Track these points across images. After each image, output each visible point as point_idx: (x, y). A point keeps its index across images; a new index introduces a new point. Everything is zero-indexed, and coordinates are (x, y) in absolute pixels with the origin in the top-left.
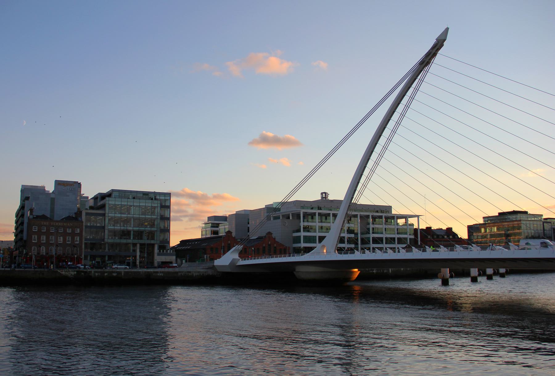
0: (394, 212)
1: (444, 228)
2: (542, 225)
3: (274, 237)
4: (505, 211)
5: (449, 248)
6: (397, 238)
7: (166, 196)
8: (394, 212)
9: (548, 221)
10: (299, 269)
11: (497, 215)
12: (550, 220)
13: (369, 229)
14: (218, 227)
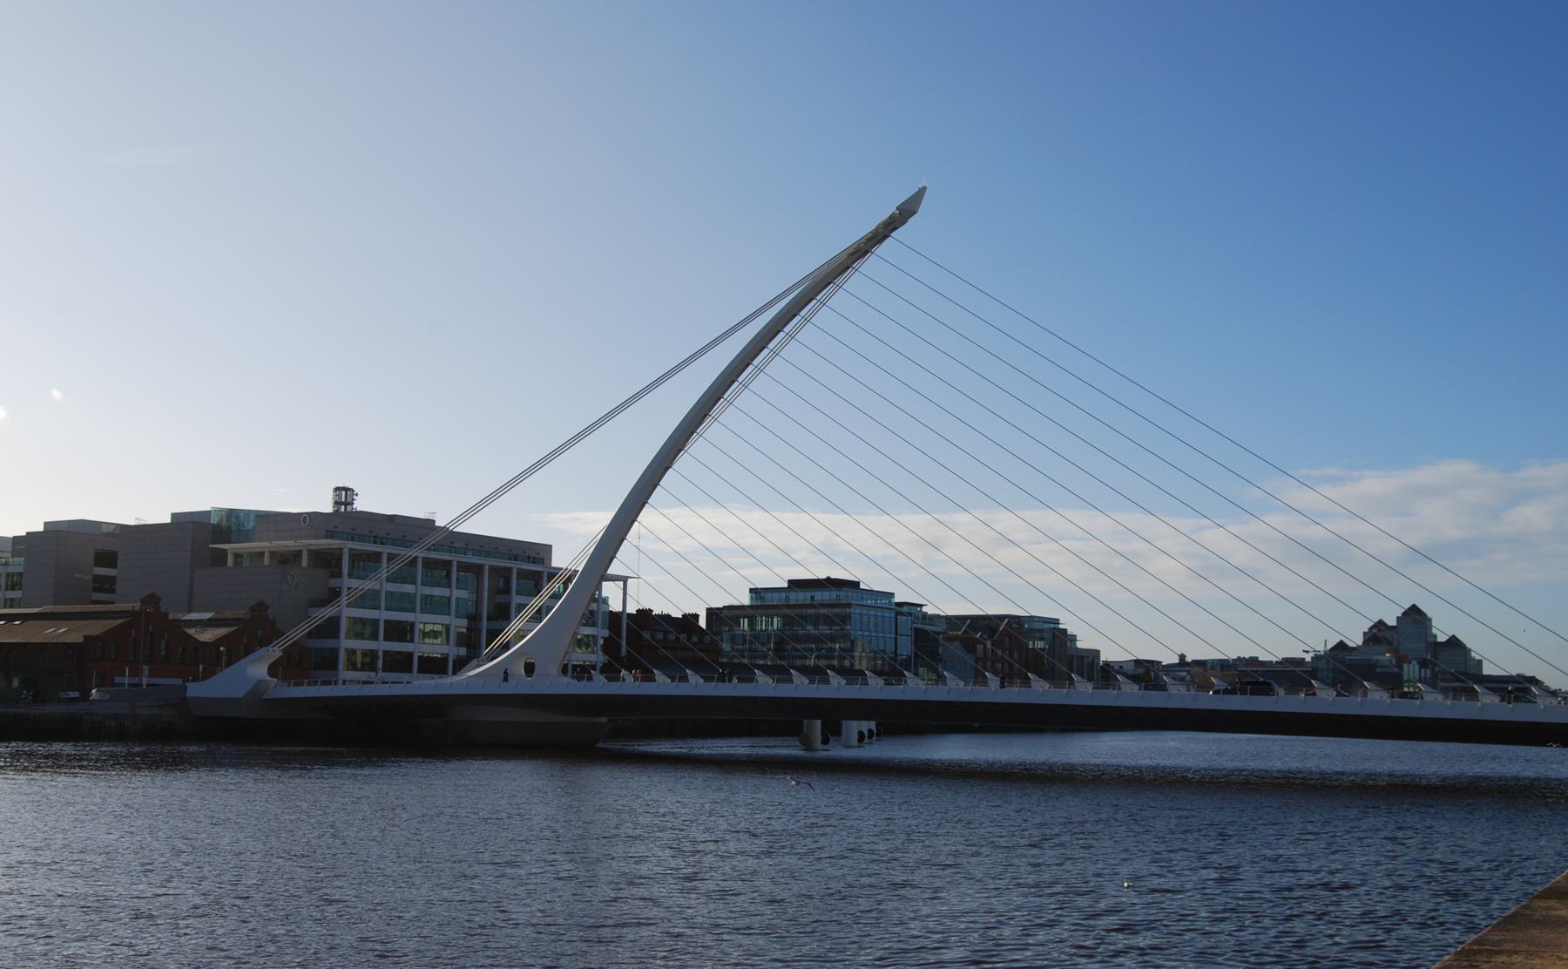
2: (893, 620)
3: (271, 618)
5: (776, 677)
9: (905, 609)
11: (786, 585)
12: (908, 607)
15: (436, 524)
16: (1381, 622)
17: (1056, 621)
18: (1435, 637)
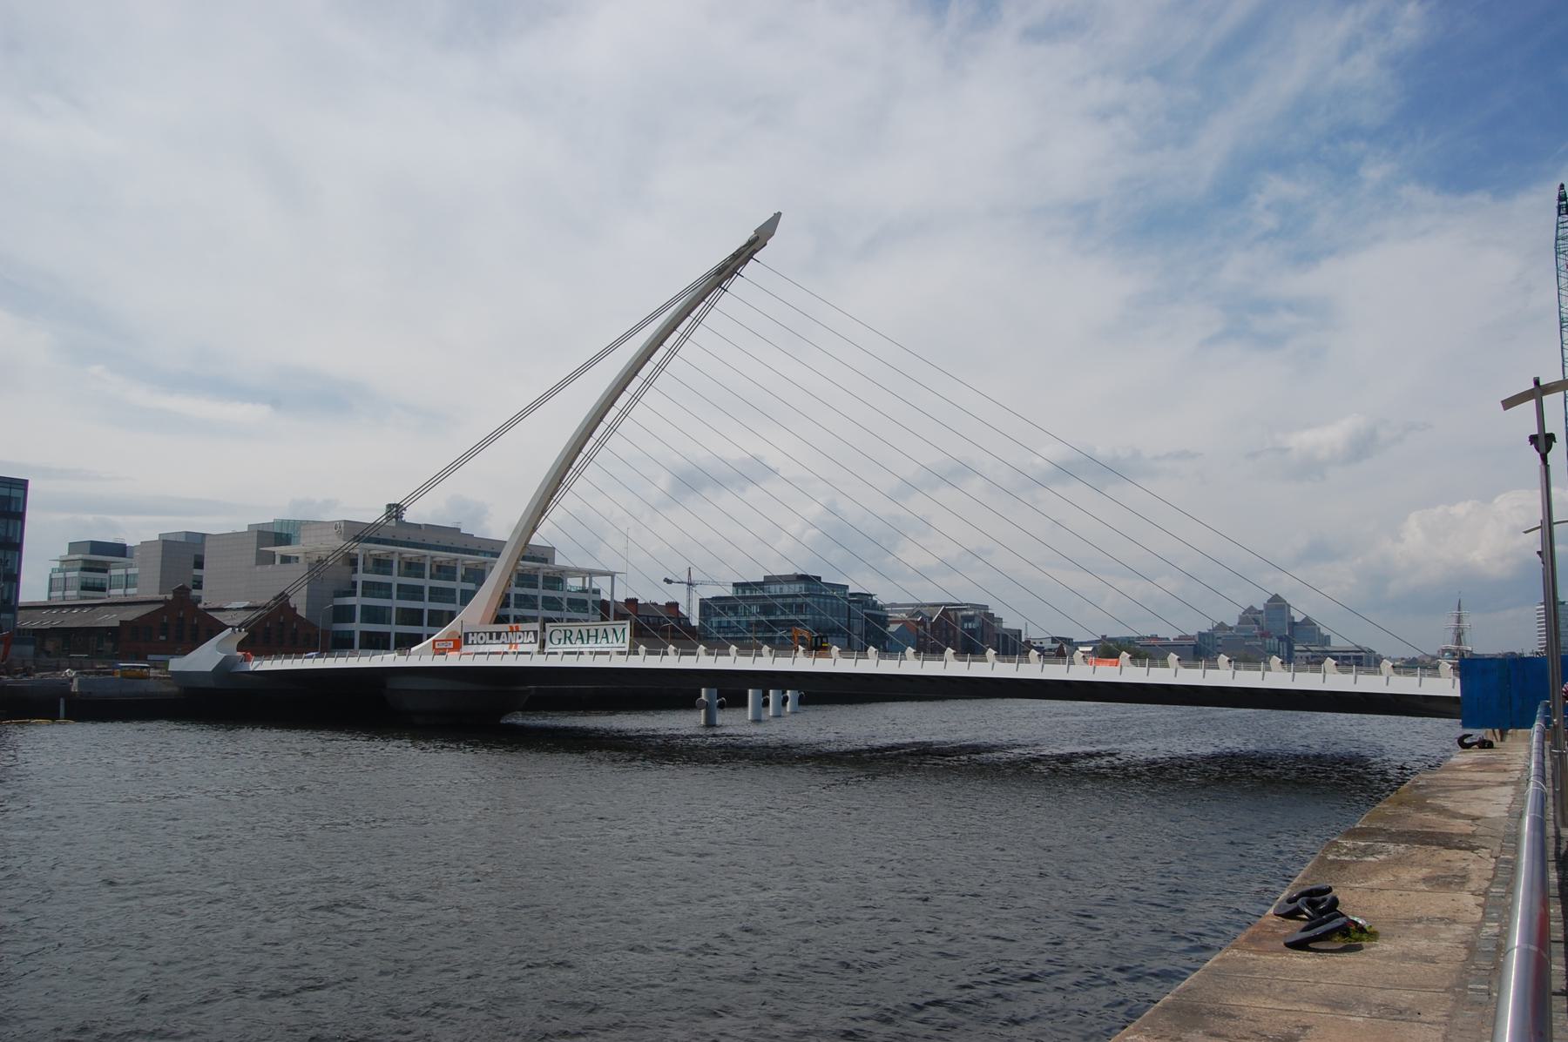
0: (560, 561)
1: (662, 603)
3: (293, 606)
4: (775, 574)
6: (429, 610)
7: (15, 486)
8: (560, 561)
11: (762, 580)
13: (354, 584)
14: (106, 571)
15: (462, 532)
16: (1252, 608)
17: (986, 607)
18: (1293, 618)
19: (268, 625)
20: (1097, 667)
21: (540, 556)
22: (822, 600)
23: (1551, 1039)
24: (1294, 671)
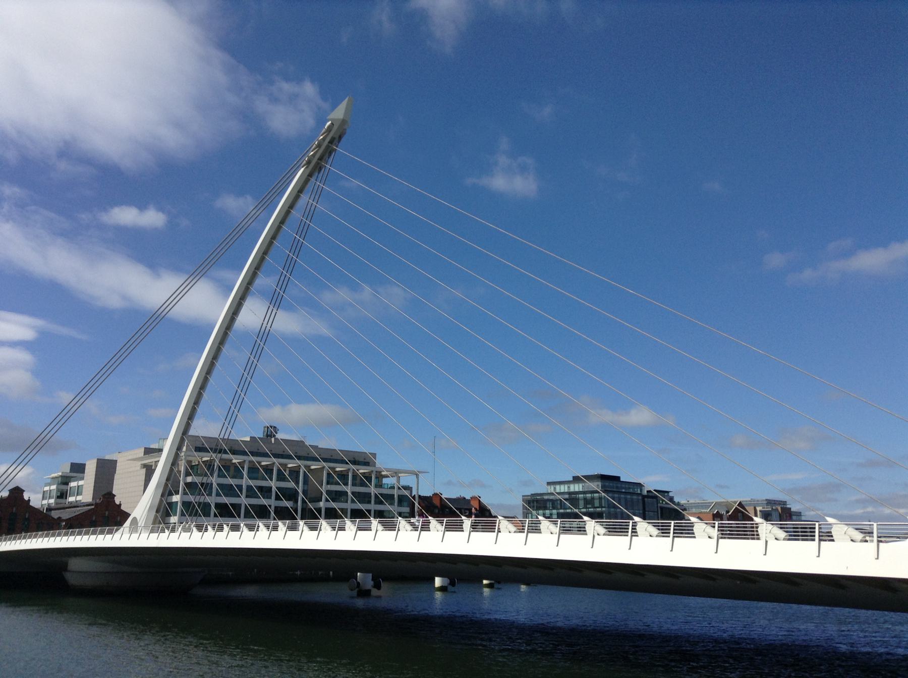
10: (75, 564)
17: (785, 503)
19: (94, 518)
20: (561, 536)
21: (362, 460)
22: (623, 496)
23: (906, 658)
24: (820, 540)
